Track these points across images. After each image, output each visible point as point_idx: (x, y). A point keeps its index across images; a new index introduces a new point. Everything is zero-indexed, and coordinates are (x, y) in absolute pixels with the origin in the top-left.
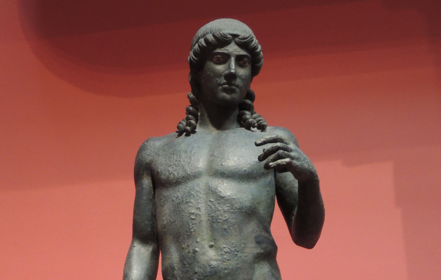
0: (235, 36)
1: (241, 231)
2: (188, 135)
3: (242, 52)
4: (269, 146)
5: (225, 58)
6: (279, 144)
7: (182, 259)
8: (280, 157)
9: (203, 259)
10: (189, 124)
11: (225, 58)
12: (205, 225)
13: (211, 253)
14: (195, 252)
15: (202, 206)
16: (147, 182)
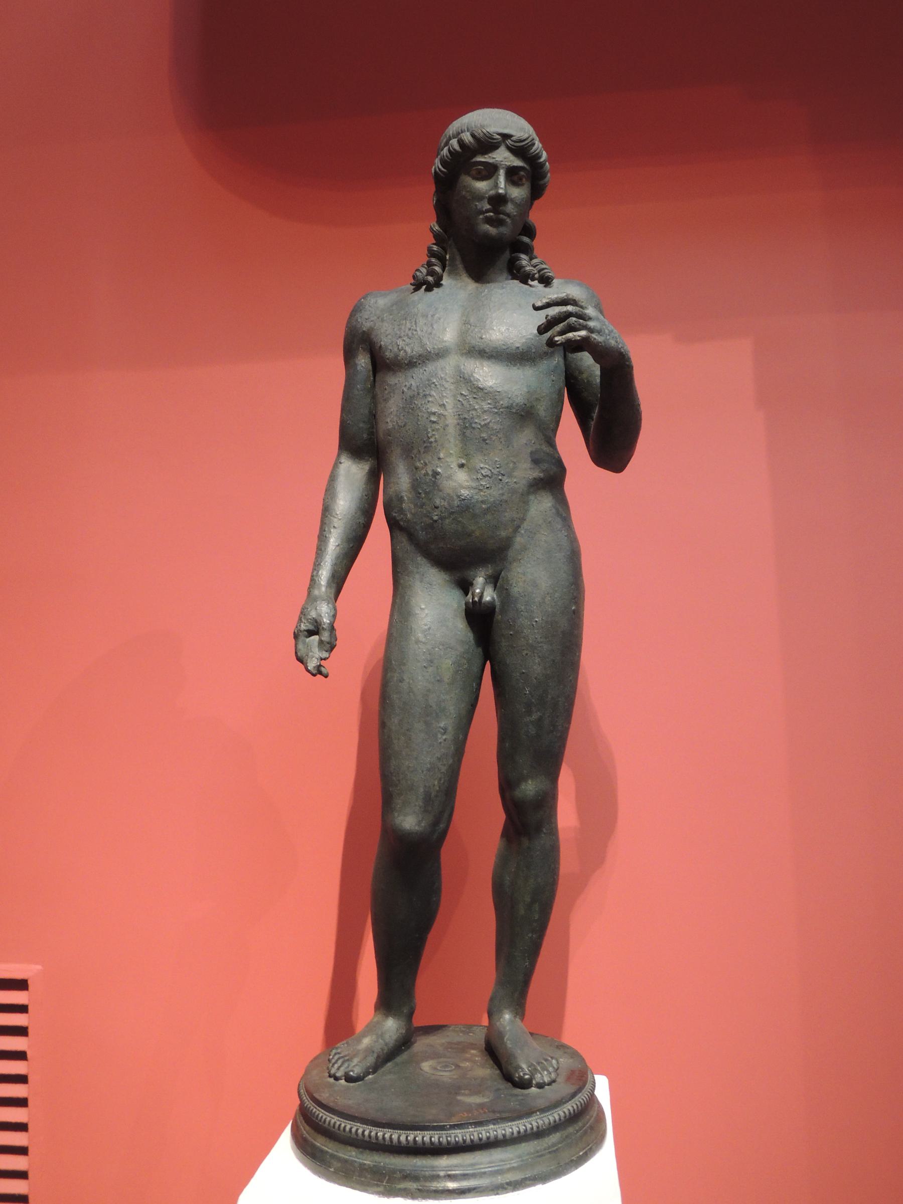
0: (506, 137)
1: (508, 443)
2: (429, 289)
3: (518, 163)
4: (554, 311)
5: (490, 171)
6: (570, 308)
7: (416, 485)
8: (572, 328)
9: (448, 486)
10: (431, 273)
11: (490, 171)
12: (452, 431)
13: (462, 477)
14: (436, 474)
15: (449, 402)
16: (363, 361)
